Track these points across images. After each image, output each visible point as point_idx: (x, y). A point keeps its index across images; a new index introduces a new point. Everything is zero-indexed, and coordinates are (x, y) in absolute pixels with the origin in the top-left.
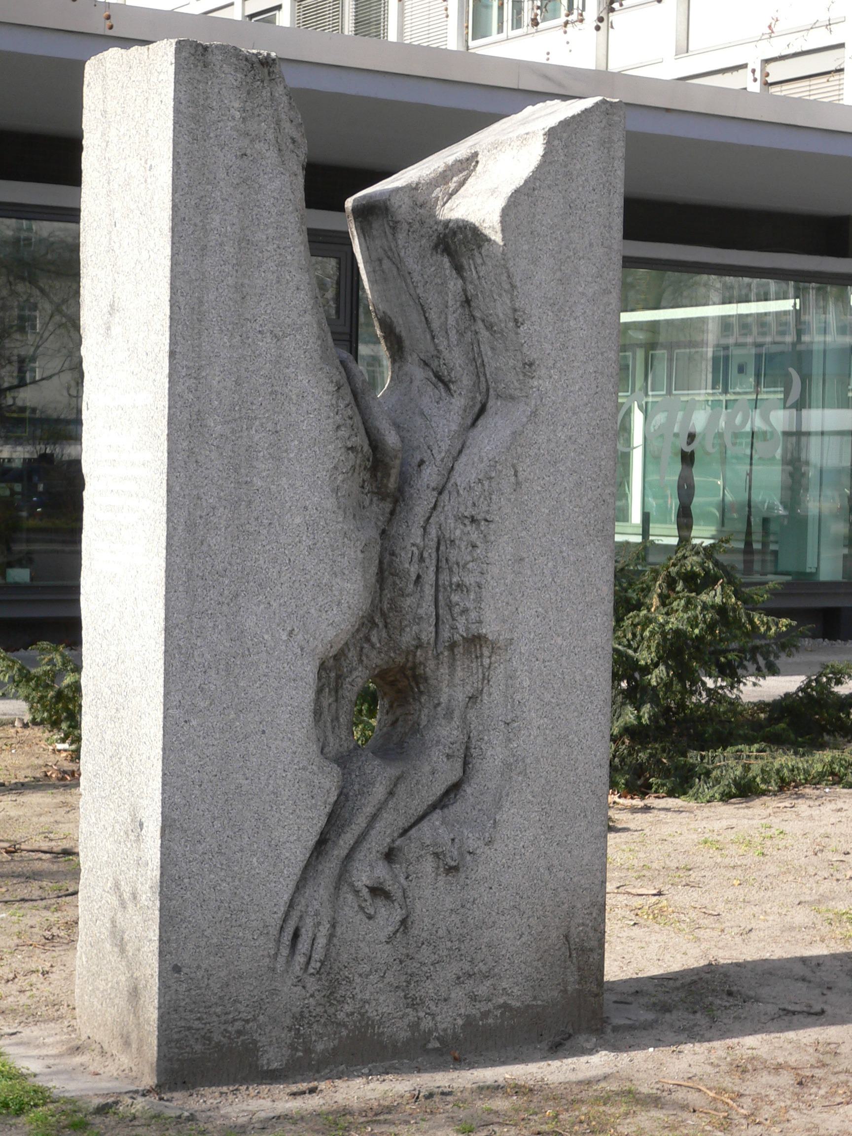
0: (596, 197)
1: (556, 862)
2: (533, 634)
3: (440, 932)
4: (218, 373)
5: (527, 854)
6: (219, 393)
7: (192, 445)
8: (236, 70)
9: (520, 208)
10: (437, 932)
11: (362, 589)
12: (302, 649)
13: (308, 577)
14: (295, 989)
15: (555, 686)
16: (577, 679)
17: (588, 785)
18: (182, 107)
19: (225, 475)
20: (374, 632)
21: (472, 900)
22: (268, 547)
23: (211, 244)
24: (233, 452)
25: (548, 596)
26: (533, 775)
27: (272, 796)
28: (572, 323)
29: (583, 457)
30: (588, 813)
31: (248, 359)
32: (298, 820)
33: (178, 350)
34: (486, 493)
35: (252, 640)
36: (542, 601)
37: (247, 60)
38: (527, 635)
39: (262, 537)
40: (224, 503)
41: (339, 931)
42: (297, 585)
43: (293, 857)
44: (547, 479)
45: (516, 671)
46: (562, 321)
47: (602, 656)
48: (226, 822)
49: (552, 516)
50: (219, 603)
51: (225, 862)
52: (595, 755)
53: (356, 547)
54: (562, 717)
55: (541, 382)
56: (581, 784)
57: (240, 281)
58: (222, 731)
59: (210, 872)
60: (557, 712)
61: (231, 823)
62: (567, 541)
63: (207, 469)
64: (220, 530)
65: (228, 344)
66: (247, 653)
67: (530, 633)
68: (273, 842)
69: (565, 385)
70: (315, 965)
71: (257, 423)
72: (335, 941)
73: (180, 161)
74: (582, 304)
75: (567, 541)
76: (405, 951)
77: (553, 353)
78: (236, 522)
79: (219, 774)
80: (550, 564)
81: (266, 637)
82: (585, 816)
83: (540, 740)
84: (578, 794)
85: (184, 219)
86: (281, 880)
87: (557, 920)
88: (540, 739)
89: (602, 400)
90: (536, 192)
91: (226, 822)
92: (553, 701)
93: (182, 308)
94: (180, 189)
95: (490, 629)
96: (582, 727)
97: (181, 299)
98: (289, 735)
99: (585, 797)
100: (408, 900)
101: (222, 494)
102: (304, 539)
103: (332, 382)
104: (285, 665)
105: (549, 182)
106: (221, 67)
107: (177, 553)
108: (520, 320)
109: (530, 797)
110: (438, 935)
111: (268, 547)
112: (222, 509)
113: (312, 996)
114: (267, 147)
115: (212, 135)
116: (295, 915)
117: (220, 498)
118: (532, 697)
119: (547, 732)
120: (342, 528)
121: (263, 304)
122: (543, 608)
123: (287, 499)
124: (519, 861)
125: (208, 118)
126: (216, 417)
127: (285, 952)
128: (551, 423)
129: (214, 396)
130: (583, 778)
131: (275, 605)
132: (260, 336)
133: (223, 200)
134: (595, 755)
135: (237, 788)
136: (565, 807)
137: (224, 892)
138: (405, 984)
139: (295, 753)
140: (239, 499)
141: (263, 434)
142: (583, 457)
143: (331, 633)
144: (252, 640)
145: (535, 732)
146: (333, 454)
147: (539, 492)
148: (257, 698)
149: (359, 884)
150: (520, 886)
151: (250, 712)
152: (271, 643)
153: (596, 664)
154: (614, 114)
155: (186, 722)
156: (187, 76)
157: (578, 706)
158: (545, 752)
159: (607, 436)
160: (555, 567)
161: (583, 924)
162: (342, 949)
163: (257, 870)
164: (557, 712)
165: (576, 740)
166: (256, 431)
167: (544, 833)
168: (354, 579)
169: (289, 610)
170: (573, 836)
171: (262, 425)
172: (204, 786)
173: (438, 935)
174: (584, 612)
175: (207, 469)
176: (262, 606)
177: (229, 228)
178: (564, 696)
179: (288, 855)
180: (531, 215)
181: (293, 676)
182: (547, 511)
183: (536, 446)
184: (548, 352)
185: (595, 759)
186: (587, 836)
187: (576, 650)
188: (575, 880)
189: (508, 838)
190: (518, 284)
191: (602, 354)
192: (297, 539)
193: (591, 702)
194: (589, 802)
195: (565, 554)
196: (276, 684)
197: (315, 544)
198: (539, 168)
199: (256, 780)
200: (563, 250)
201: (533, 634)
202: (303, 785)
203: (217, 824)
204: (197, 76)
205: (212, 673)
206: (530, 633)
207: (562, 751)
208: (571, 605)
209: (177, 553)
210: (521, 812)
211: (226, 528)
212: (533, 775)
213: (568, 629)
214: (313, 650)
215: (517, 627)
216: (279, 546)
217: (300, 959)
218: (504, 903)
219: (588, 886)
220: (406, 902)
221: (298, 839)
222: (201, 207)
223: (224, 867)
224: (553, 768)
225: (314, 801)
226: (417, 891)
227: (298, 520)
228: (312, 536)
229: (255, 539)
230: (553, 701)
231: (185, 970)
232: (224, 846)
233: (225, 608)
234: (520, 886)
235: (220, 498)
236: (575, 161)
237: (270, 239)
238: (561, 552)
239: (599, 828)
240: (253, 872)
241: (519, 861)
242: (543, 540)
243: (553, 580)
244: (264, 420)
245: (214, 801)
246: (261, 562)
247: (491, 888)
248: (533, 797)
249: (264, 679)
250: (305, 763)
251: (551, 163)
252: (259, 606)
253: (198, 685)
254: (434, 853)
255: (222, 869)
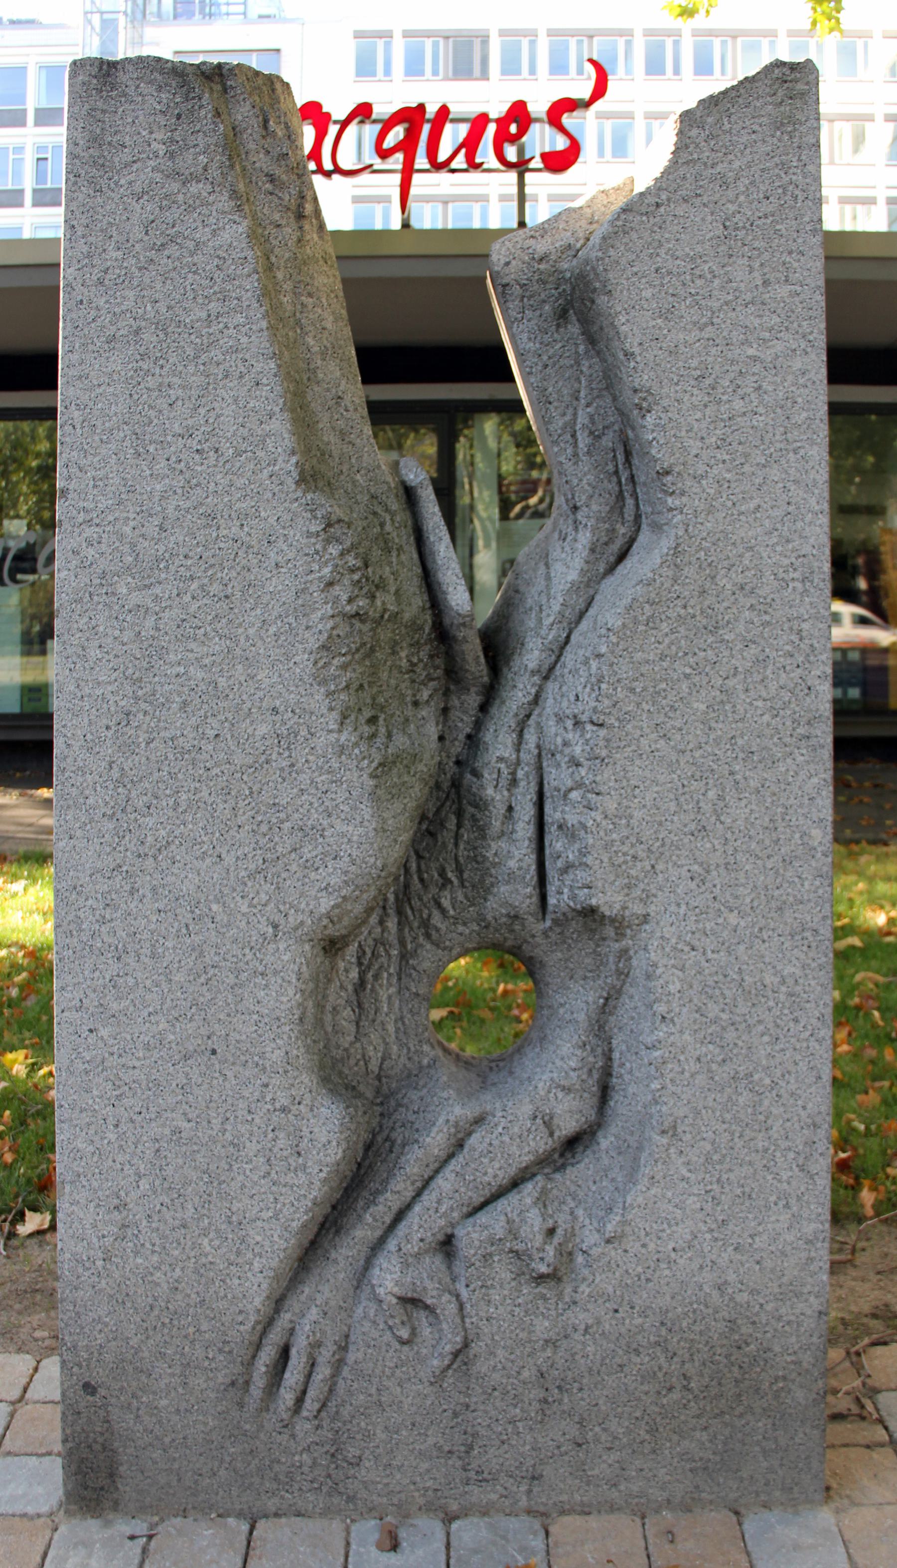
0: (770, 209)
1: (732, 1277)
2: (683, 907)
3: (526, 1374)
4: (132, 516)
5: (681, 1262)
6: (133, 545)
7: (93, 622)
8: (160, 89)
9: (634, 235)
10: (518, 1373)
11: (372, 834)
12: (276, 927)
13: (282, 815)
14: (279, 1438)
15: (727, 993)
16: (767, 981)
17: (791, 1155)
18: (78, 150)
19: (145, 664)
20: (446, 893)
21: (583, 1327)
22: (216, 771)
23: (121, 332)
24: (158, 629)
25: (708, 845)
26: (689, 1136)
27: (231, 1149)
28: (738, 405)
29: (767, 618)
30: (793, 1202)
31: (179, 491)
32: (274, 1188)
33: (71, 487)
34: (593, 680)
35: (192, 912)
36: (698, 853)
37: (445, 711)
38: (673, 908)
39: (205, 756)
40: (144, 706)
41: (351, 1357)
42: (264, 828)
43: (267, 1243)
44: (702, 654)
45: (655, 965)
46: (719, 402)
47: (814, 945)
48: (157, 1183)
49: (713, 715)
50: (139, 856)
51: (158, 1242)
52: (804, 1108)
53: (362, 770)
54: (740, 1043)
55: (684, 499)
56: (778, 1154)
57: (167, 381)
58: (147, 1047)
59: (136, 1253)
60: (730, 1035)
61: (166, 1185)
62: (741, 755)
63: (116, 656)
64: (138, 746)
65: (148, 472)
66: (184, 931)
67: (678, 905)
68: (234, 1218)
69: (729, 504)
70: (310, 1405)
71: (195, 585)
72: (345, 1371)
73: (75, 223)
74: (754, 374)
75: (741, 755)
76: (463, 1399)
77: (705, 454)
78: (162, 734)
79: (144, 1111)
80: (711, 794)
81: (215, 907)
82: (787, 1206)
83: (701, 1079)
84: (775, 1170)
85: (81, 302)
86: (249, 1274)
87: (735, 1369)
88: (701, 1079)
89: (799, 524)
90: (662, 209)
91: (157, 1183)
92: (724, 1016)
93: (78, 426)
94: (75, 261)
95: (609, 900)
96: (778, 1060)
97: (76, 414)
98: (256, 1058)
99: (785, 1175)
100: (467, 1320)
101: (140, 693)
102: (274, 757)
103: (315, 518)
104: (247, 951)
105: (684, 193)
106: (138, 87)
107: (72, 781)
108: (645, 405)
109: (684, 1172)
110: (521, 1378)
111: (216, 771)
112: (141, 716)
113: (308, 1449)
114: (209, 188)
115: (122, 182)
116: (285, 1318)
117: (137, 699)
118: (685, 1010)
119: (714, 1067)
120: (338, 740)
121: (202, 411)
122: (701, 864)
123: (245, 697)
124: (667, 1272)
125: (117, 160)
126: (130, 580)
127: (259, 1380)
128: (705, 564)
129: (126, 549)
130: (784, 1144)
131: (229, 860)
132: (197, 457)
133: (140, 269)
134: (804, 1108)
135: (174, 1132)
136: (747, 1190)
137: (158, 1284)
138: (463, 1448)
139: (266, 1086)
140: (167, 700)
141: (205, 601)
142: (767, 618)
143: (326, 904)
144: (192, 912)
145: (693, 1066)
146: (320, 626)
147: (687, 676)
148: (202, 999)
149: (381, 1291)
150: (667, 1311)
151: (191, 1020)
152: (221, 918)
153: (802, 956)
154: (796, 81)
155: (91, 1031)
156: (87, 107)
157: (771, 1025)
158: (710, 1099)
159: (812, 582)
160: (721, 798)
161: (784, 1378)
162: (355, 1385)
163: (210, 1258)
164: (730, 1035)
165: (767, 1081)
166: (193, 598)
167: (711, 1231)
168: (359, 819)
169: (252, 867)
170: (765, 1237)
171: (202, 587)
172: (123, 1127)
173: (521, 1378)
174: (777, 872)
175: (116, 656)
176: (208, 861)
177: (149, 308)
178: (745, 1010)
179: (259, 1238)
180: (656, 244)
181: (261, 969)
182: (703, 707)
183: (679, 602)
184: (694, 452)
185: (803, 1114)
186: (790, 1238)
187: (765, 935)
188: (769, 1307)
189: (647, 1234)
190: (636, 350)
191: (795, 451)
192: (263, 758)
193: (796, 1020)
194: (794, 1183)
195: (738, 777)
196: (231, 980)
197: (292, 765)
198: (666, 172)
199: (205, 1123)
200: (715, 293)
201: (683, 907)
202: (282, 1135)
203: (144, 1185)
204: (100, 104)
205: (131, 960)
206: (678, 905)
207: (741, 1100)
208: (752, 860)
209: (72, 781)
210: (669, 1194)
211: (148, 743)
212: (689, 1136)
213: (748, 900)
214: (296, 929)
215: (655, 896)
216: (233, 768)
217: (287, 1397)
218: (640, 1337)
219: (793, 1318)
220: (463, 1322)
221: (276, 1216)
222: (107, 282)
223: (157, 1248)
224: (725, 1126)
225: (300, 1160)
226: (485, 1308)
227: (263, 729)
228: (287, 754)
229: (194, 759)
230: (724, 1016)
231: (102, 1392)
232: (156, 1218)
233: (150, 863)
234: (667, 1311)
235: (137, 699)
236: (731, 157)
237: (213, 317)
238: (732, 773)
239: (813, 1226)
240: (204, 1260)
241: (667, 1272)
242: (697, 754)
243: (718, 819)
244: (206, 581)
245: (138, 1151)
246: (205, 793)
247: (616, 1311)
248: (690, 1171)
249: (211, 972)
250: (285, 1102)
251: (687, 163)
252: (203, 859)
253: (108, 977)
254: (511, 1251)
255: (153, 1252)
